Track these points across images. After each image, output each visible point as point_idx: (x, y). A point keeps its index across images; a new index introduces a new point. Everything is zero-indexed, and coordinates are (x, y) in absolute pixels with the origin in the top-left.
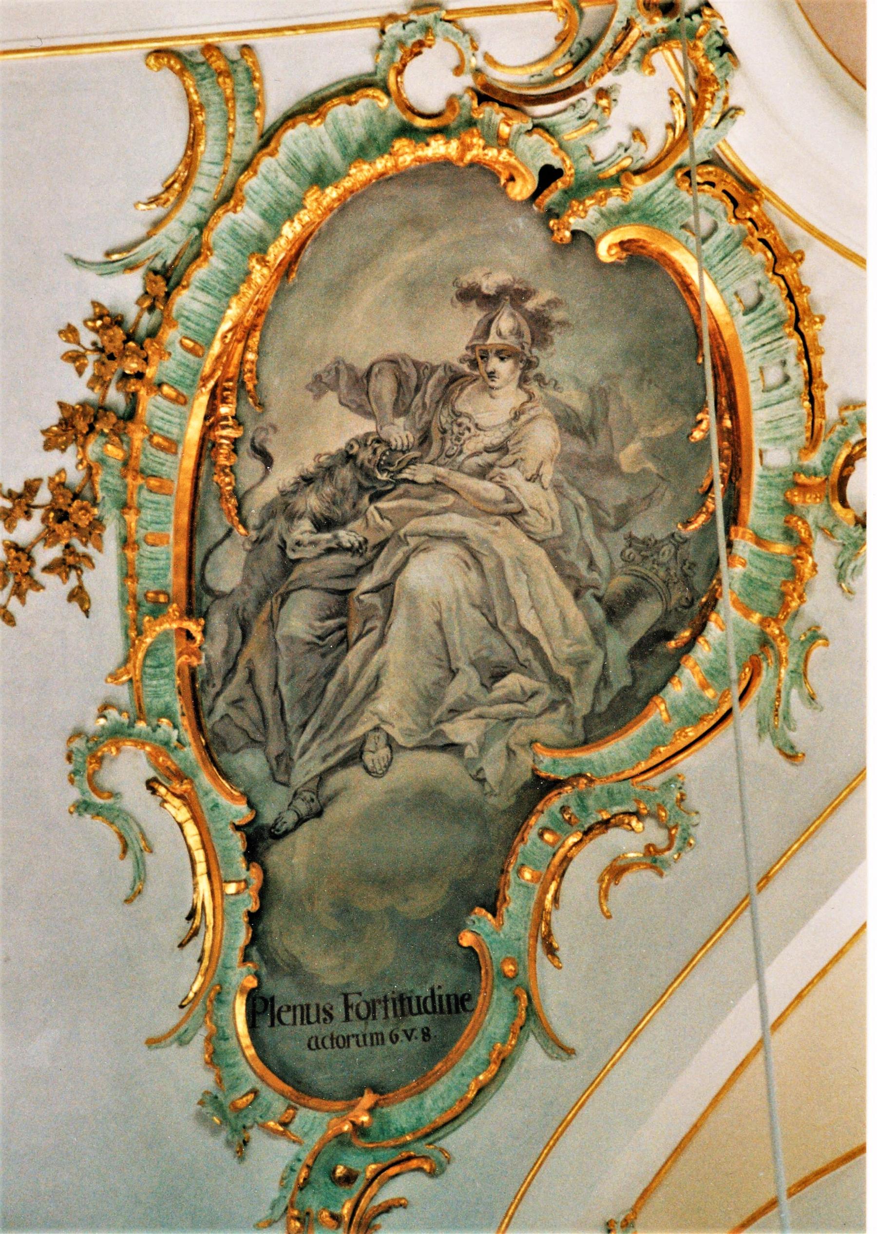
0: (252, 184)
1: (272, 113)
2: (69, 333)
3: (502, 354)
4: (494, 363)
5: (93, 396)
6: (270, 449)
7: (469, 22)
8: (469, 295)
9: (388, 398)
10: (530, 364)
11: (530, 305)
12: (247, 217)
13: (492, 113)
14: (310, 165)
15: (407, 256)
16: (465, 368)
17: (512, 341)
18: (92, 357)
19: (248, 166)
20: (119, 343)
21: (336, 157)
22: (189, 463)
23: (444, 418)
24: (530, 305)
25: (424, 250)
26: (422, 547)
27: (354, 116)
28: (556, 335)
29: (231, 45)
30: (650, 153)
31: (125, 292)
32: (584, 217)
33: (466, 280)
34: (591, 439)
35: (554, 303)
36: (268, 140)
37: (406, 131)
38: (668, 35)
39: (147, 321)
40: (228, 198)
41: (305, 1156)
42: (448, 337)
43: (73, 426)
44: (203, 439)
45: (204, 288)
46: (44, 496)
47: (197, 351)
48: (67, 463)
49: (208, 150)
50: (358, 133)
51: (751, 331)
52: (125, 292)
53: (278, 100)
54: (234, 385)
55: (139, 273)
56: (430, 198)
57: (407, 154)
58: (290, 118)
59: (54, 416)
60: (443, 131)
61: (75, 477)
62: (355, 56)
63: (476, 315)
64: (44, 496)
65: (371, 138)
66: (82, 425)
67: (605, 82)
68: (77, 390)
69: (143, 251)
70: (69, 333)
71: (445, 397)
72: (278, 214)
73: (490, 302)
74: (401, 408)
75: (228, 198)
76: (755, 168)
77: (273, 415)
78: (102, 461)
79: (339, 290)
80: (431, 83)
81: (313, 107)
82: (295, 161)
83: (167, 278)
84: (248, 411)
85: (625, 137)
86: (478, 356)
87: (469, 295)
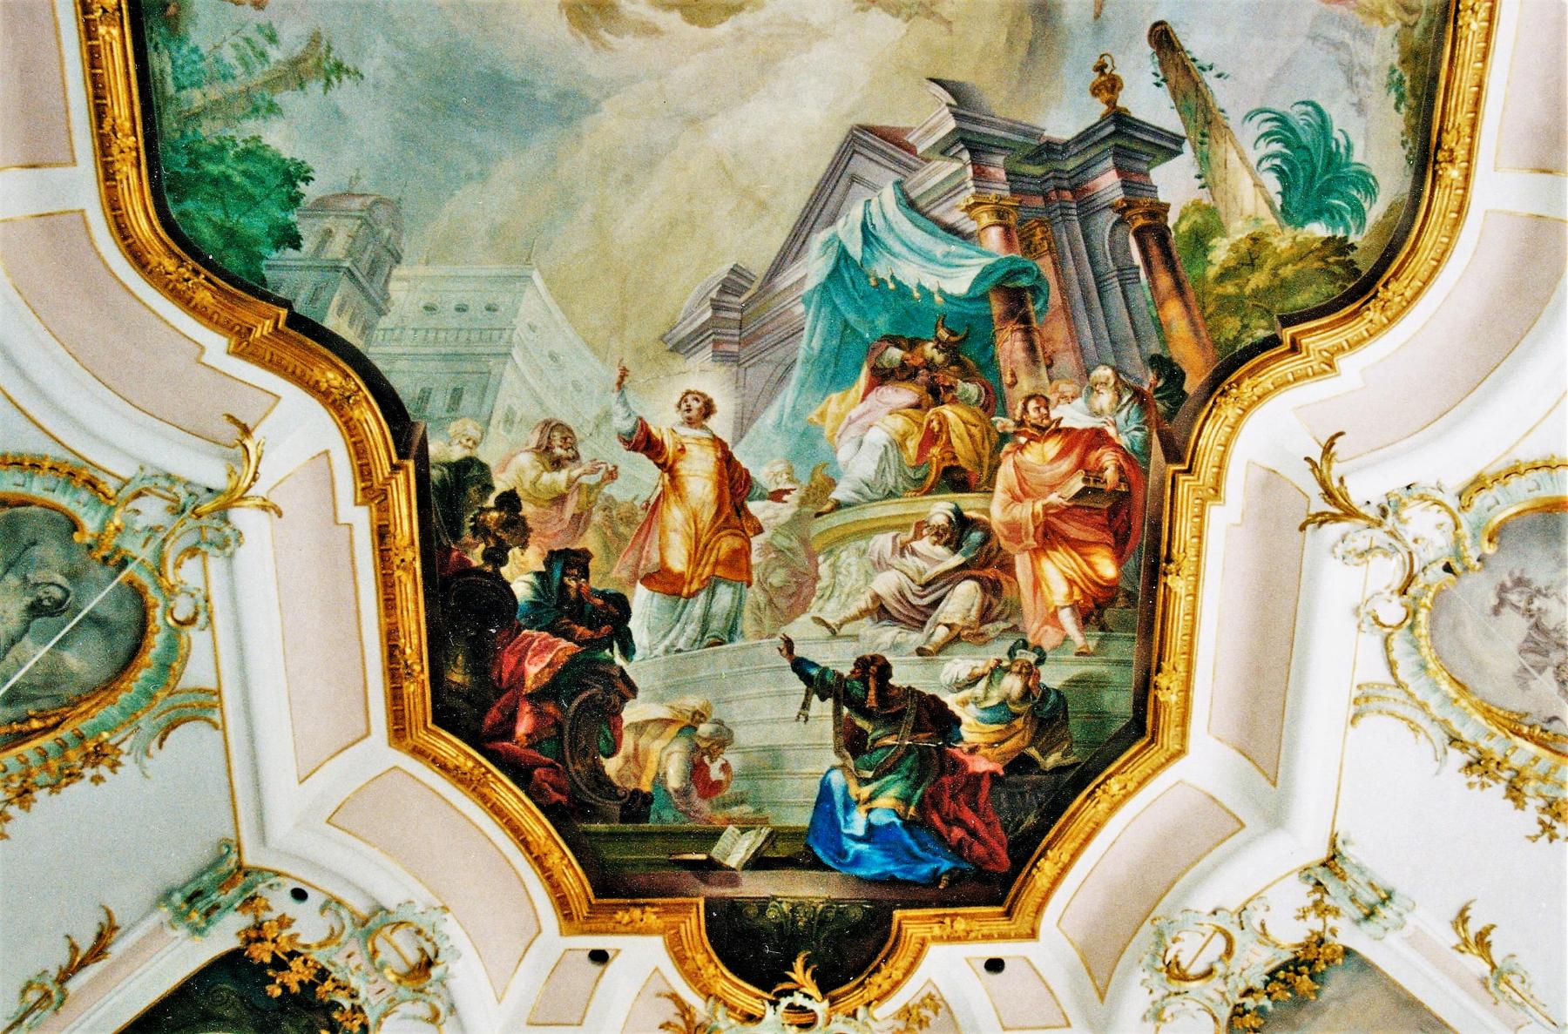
0: (1419, 696)
1: (1391, 681)
2: (1470, 785)
3: (1530, 602)
4: (1534, 607)
5: (1503, 784)
6: (1551, 715)
7: (1368, 595)
8: (1496, 611)
9: (1539, 658)
10: (1539, 591)
11: (1509, 584)
12: (1433, 701)
13: (1412, 591)
14: (1416, 669)
15: (1470, 633)
16: (1533, 620)
17: (1525, 597)
18: (1485, 779)
19: (1411, 695)
20: (1479, 764)
21: (1415, 658)
22: (1547, 753)
23: (1555, 635)
24: (1509, 584)
25: (1469, 628)
26: (983, 684)
27: (1399, 644)
28: (1527, 576)
29: (1356, 693)
30: (1449, 520)
31: (1457, 758)
32: (1472, 555)
33: (1489, 611)
34: (1473, 728)
35: (1511, 574)
36: (1399, 685)
37: (1411, 628)
38: (1396, 513)
39: (1473, 751)
40: (1423, 706)
41: (779, 468)
42: (1515, 626)
43: (1515, 792)
44: (1536, 743)
45: (1463, 725)
46: (1547, 819)
47: (1492, 736)
48: (1533, 804)
49: (1400, 710)
50: (1408, 647)
51: (1550, 488)
52: (1457, 758)
53: (1383, 675)
54: (1514, 725)
55: (1450, 749)
56: (1444, 621)
57: (1422, 630)
58: (1393, 674)
59: (1509, 802)
60: (1415, 613)
61: (1541, 803)
62: (1374, 641)
63: (1506, 610)
64: (1547, 819)
65: (1411, 642)
66: (1516, 794)
67: (1409, 540)
68: (1500, 789)
69: (1440, 747)
70: (1470, 785)
71: (1545, 633)
72: (1436, 687)
73: (1502, 602)
74: (1546, 654)
75: (1423, 706)
76: (1469, 476)
77: (1533, 710)
78: (1536, 790)
79: (1480, 668)
80: (1392, 612)
81: (1392, 665)
82: (1413, 675)
83: (1454, 740)
84: (1528, 720)
85: (1438, 533)
86: (1529, 613)
87: (1496, 611)
